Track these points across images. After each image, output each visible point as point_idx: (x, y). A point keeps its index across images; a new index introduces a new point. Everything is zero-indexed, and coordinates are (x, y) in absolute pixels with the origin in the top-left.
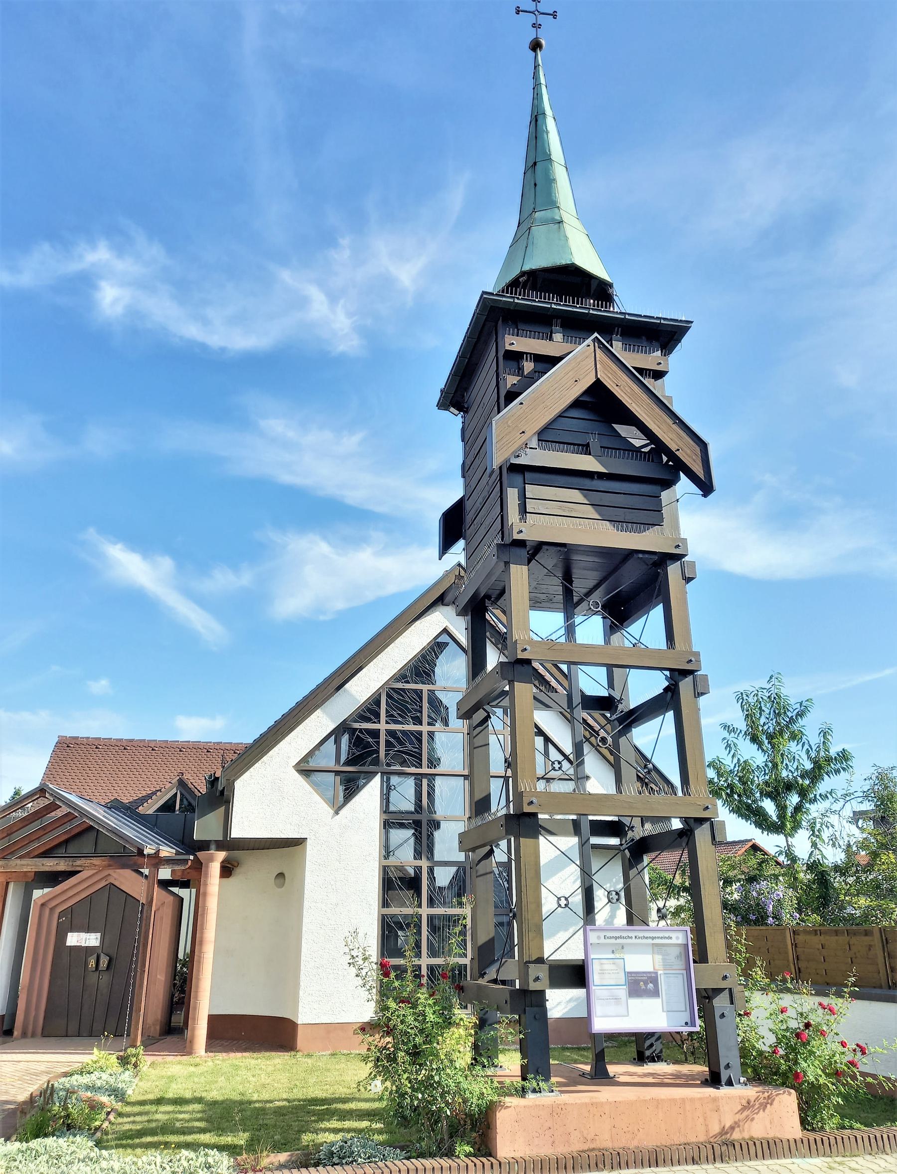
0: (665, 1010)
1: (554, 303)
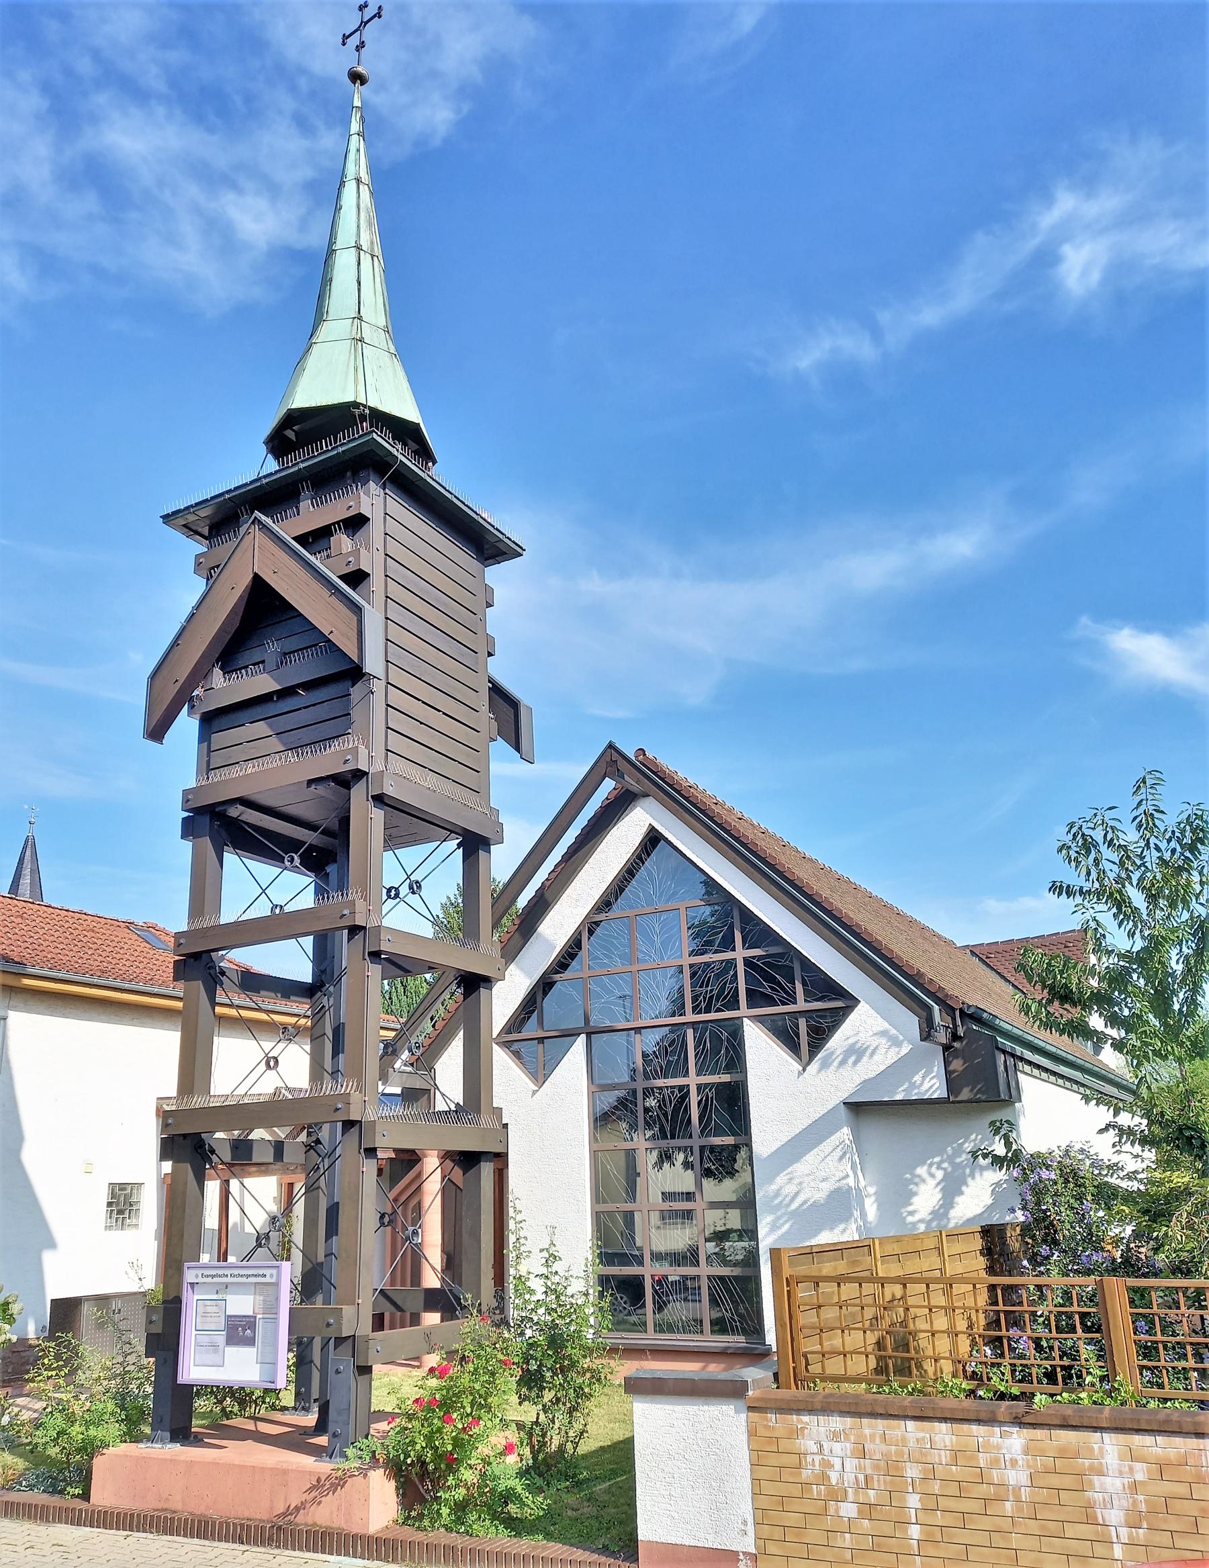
0: (259, 1361)
1: (302, 462)
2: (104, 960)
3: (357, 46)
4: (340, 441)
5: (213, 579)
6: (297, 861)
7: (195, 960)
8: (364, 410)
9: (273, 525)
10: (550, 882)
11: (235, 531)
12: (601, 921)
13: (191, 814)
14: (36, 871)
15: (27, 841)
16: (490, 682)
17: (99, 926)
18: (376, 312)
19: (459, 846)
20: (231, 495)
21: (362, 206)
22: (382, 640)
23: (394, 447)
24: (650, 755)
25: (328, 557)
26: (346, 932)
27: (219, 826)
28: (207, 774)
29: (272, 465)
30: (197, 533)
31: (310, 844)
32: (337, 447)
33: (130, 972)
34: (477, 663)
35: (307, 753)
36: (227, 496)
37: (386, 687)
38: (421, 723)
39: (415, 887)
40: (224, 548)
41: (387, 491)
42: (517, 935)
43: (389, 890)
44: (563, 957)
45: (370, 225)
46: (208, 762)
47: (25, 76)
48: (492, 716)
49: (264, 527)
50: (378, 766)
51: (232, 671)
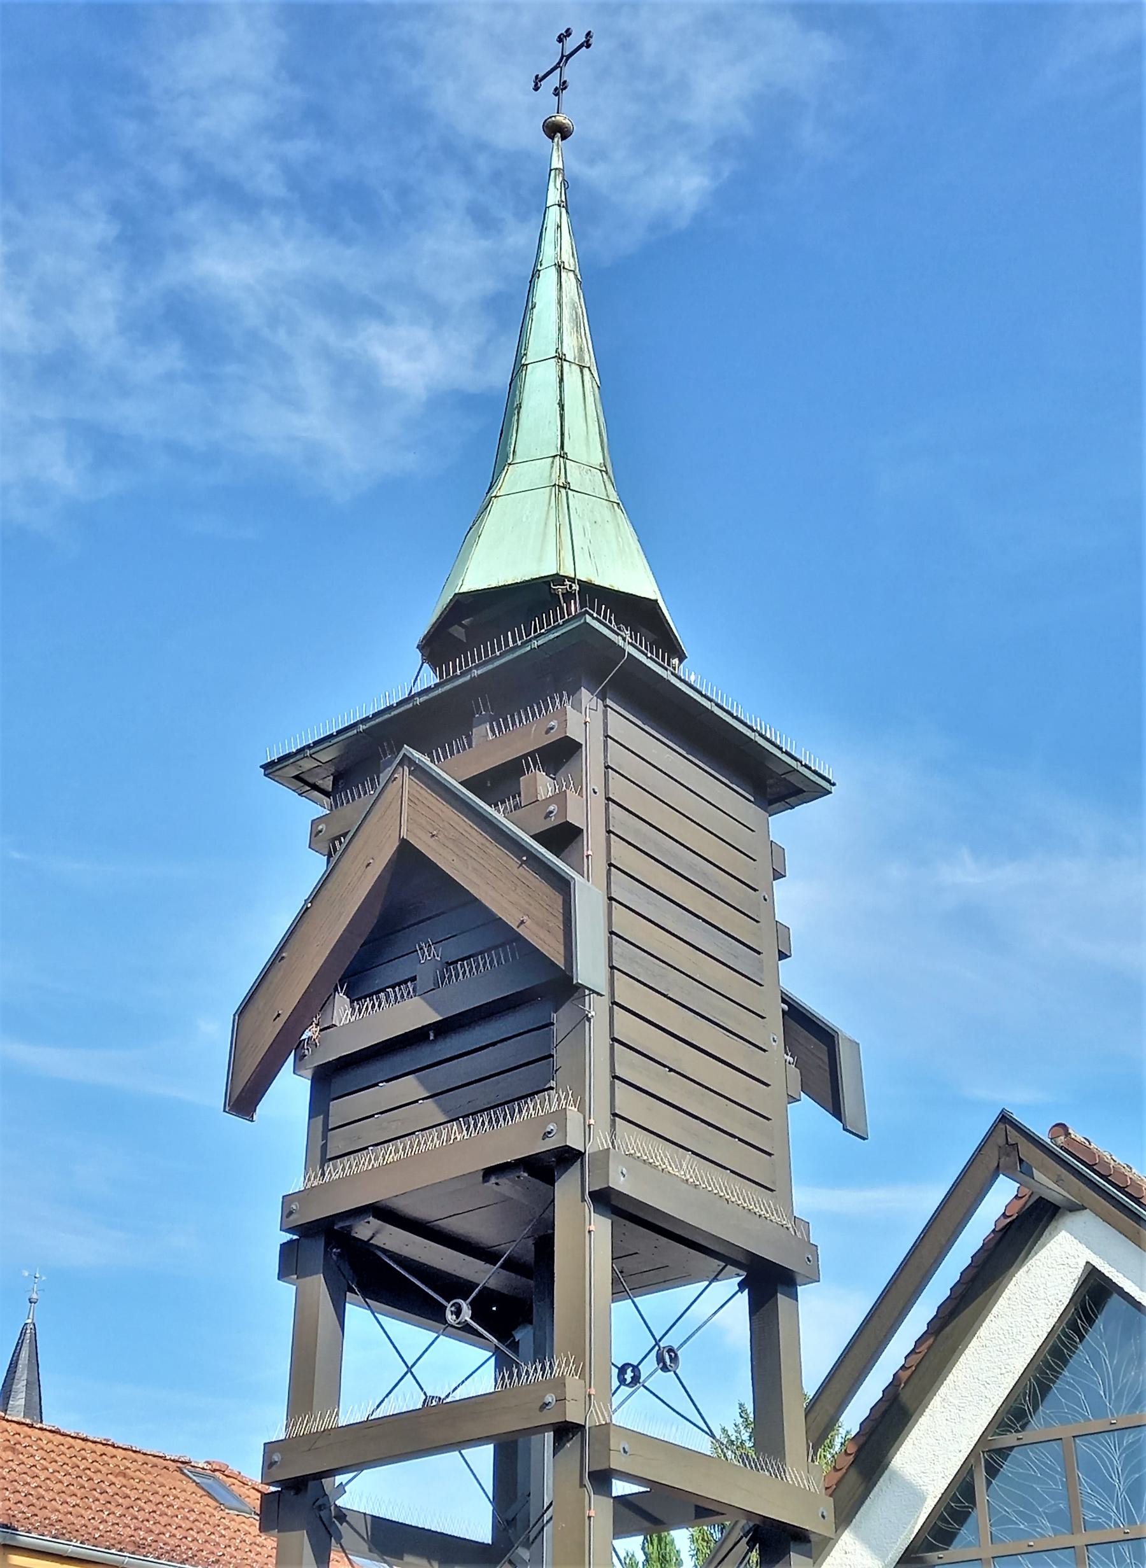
1: (477, 667)
2: (141, 1525)
3: (556, 89)
4: (535, 631)
5: (338, 854)
6: (467, 1314)
7: (296, 1494)
8: (571, 587)
9: (432, 765)
10: (909, 1372)
11: (372, 780)
12: (1011, 1448)
13: (295, 1237)
14: (35, 1385)
15: (23, 1333)
16: (784, 1001)
17: (134, 1466)
18: (588, 445)
19: (742, 1286)
20: (368, 725)
21: (565, 300)
22: (603, 935)
23: (618, 634)
24: (1077, 1134)
25: (516, 807)
26: (549, 1436)
27: (339, 1255)
28: (322, 1167)
29: (429, 678)
30: (315, 787)
31: (484, 1288)
32: (530, 640)
33: (183, 1548)
34: (761, 970)
35: (483, 1123)
36: (362, 727)
37: (611, 1011)
38: (671, 1070)
39: (667, 1359)
40: (352, 810)
41: (609, 702)
42: (853, 1475)
43: (622, 1370)
44: (942, 1518)
45: (578, 327)
46: (324, 1148)
47: (88, 197)
48: (789, 1058)
49: (419, 771)
50: (598, 1142)
51: (365, 997)
